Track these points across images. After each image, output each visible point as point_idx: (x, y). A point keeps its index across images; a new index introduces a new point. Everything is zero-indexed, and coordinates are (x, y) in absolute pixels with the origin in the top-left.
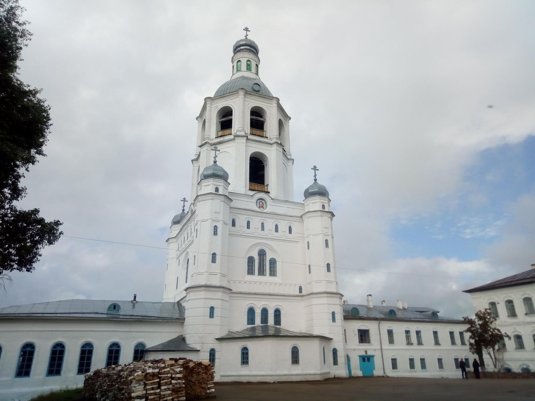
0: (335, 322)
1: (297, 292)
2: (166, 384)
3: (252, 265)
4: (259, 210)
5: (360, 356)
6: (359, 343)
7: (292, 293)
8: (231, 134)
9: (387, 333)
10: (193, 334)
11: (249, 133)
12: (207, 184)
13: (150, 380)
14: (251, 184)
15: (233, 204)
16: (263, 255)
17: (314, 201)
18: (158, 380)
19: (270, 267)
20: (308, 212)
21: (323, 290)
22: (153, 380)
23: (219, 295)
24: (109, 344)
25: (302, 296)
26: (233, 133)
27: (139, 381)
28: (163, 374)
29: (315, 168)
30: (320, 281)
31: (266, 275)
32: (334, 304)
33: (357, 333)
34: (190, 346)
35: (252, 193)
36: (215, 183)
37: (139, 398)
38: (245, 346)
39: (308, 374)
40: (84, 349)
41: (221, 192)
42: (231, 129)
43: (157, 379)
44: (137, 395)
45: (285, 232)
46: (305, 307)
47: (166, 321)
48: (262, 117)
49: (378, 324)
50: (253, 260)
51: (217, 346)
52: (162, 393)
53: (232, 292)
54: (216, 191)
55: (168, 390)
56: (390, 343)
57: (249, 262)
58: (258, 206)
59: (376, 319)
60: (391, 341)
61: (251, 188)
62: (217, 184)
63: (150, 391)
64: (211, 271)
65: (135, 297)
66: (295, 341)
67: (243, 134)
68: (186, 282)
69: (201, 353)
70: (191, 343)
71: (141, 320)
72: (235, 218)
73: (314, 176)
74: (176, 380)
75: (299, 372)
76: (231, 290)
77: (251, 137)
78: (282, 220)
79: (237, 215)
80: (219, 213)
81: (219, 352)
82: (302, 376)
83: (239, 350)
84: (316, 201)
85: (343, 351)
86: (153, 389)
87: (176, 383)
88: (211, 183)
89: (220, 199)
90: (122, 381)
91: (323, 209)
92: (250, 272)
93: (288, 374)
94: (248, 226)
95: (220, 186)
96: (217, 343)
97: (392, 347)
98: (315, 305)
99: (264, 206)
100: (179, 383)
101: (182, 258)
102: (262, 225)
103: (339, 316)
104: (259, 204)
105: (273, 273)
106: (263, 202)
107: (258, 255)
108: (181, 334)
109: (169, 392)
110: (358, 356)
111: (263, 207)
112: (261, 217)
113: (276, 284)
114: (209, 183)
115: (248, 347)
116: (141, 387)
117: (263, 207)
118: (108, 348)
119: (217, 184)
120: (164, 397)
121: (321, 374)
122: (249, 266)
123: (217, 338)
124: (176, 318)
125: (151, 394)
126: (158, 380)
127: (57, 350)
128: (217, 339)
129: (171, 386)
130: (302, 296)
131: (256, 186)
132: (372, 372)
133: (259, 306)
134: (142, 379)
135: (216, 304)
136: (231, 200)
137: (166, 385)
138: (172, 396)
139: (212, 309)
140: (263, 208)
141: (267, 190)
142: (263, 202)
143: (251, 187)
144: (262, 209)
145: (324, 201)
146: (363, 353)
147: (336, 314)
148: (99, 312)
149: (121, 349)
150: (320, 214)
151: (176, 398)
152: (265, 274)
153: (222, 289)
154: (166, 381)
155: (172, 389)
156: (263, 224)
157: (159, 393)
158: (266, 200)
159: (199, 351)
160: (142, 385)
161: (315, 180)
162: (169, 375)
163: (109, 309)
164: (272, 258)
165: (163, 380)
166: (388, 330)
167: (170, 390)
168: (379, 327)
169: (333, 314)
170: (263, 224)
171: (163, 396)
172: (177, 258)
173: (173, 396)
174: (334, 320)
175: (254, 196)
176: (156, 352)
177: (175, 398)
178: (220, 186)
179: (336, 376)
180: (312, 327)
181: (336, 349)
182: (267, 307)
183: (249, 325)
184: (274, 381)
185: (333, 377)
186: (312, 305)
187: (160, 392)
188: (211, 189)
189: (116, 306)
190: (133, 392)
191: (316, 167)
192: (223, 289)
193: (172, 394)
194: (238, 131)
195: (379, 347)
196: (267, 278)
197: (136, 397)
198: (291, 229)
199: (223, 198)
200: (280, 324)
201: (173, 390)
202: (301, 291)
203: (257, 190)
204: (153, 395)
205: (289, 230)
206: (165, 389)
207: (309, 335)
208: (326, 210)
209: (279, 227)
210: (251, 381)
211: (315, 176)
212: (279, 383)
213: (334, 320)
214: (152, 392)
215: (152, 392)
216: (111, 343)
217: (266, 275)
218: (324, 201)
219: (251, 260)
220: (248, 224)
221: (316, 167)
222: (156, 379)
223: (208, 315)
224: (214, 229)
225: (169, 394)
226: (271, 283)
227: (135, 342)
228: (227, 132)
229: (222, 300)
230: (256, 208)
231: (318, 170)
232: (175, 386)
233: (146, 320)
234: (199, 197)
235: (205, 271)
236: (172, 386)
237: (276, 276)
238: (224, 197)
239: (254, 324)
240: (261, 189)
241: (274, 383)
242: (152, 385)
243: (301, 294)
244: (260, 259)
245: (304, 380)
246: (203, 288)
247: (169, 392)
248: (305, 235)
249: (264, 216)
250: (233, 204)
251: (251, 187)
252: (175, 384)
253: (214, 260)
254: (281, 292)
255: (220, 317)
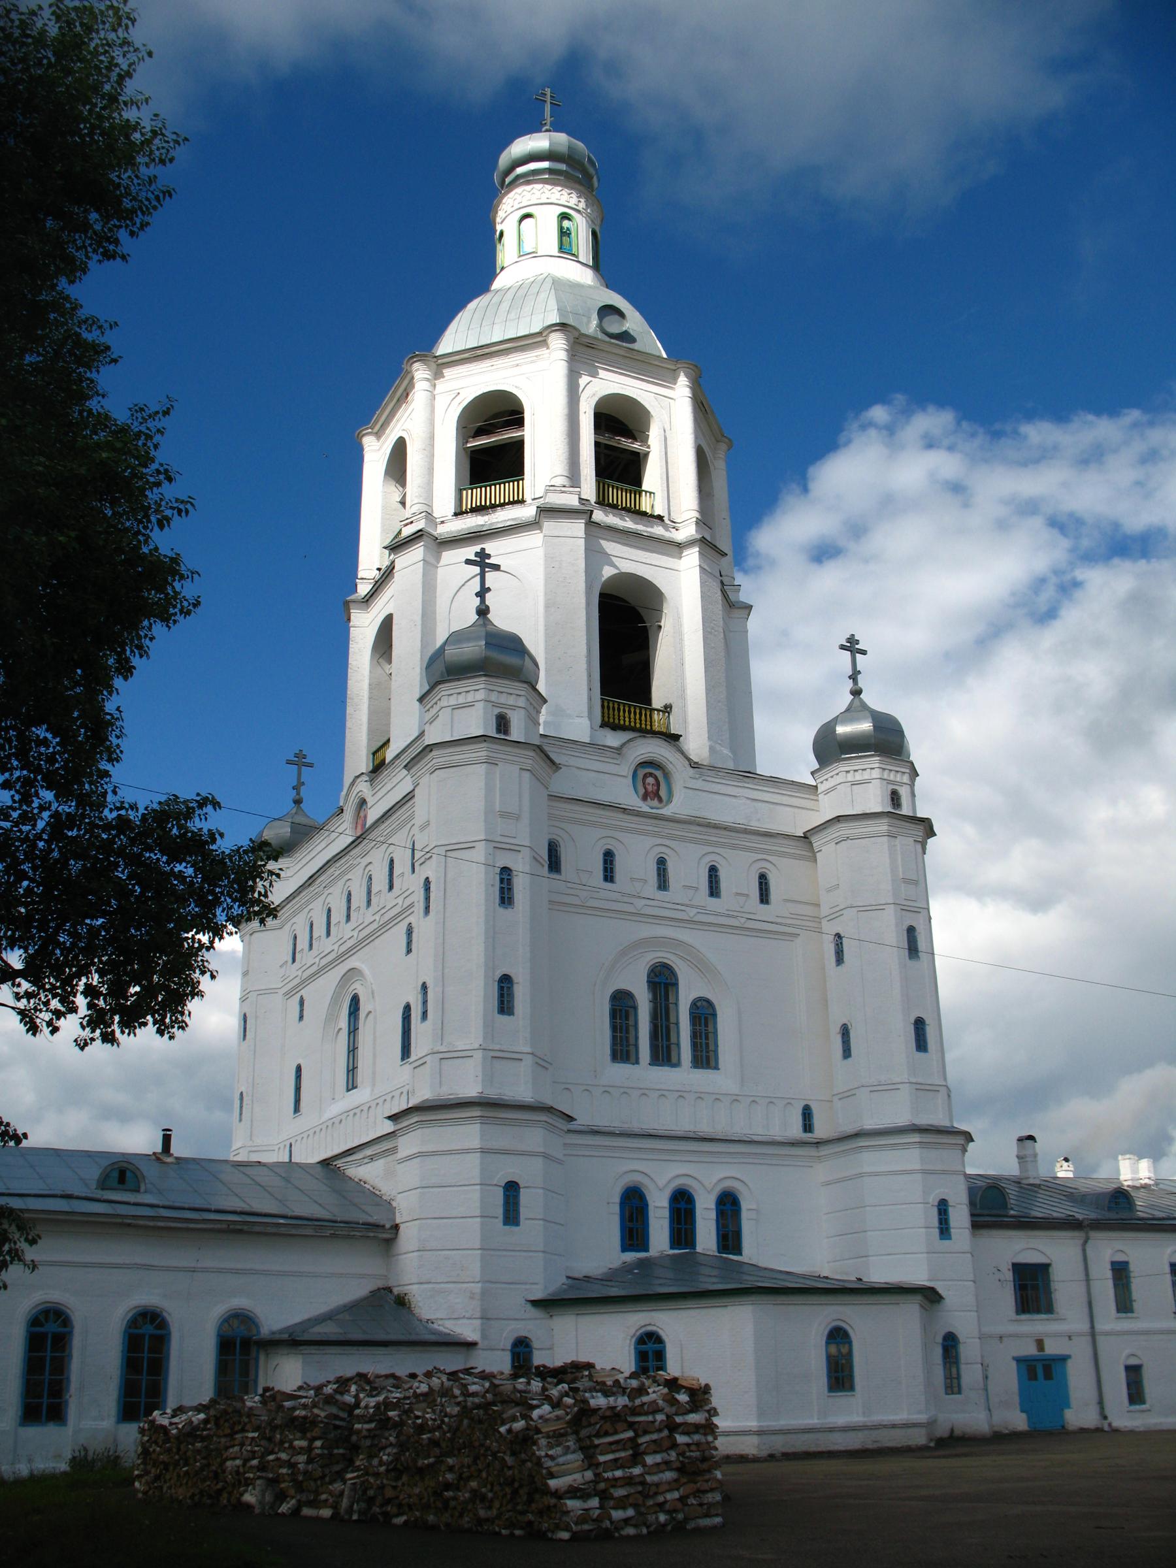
0: (950, 1239)
1: (795, 1130)
2: (657, 1447)
3: (627, 1026)
4: (644, 807)
5: (1019, 1360)
6: (1018, 1313)
7: (777, 1131)
8: (521, 502)
9: (1109, 1274)
10: (442, 1285)
11: (593, 499)
12: (461, 699)
13: (606, 1434)
14: (606, 704)
15: (562, 784)
16: (667, 985)
17: (858, 777)
18: (630, 1434)
19: (695, 1035)
20: (838, 819)
21: (903, 1120)
22: (616, 1432)
23: (534, 1137)
24: (126, 1314)
25: (818, 1144)
26: (528, 497)
27: (557, 1437)
28: (640, 1414)
29: (852, 646)
30: (892, 1087)
31: (677, 1064)
32: (944, 1172)
33: (1009, 1275)
34: (435, 1326)
35: (613, 739)
36: (494, 697)
37: (578, 1494)
38: (650, 1328)
39: (885, 1426)
40: (136, 1331)
41: (516, 734)
42: (523, 479)
43: (625, 1431)
44: (571, 1486)
45: (747, 895)
46: (828, 1184)
47: (328, 1233)
48: (631, 435)
49: (1081, 1242)
50: (631, 1003)
51: (534, 1326)
52: (648, 1478)
53: (573, 1126)
54: (499, 731)
55: (663, 1467)
56: (1118, 1311)
57: (614, 1014)
58: (642, 791)
59: (1070, 1224)
60: (1124, 1304)
61: (606, 719)
62: (503, 699)
63: (612, 1470)
64: (497, 1047)
65: (167, 1140)
66: (840, 1308)
67: (572, 501)
68: (351, 1086)
69: (481, 1352)
70: (439, 1315)
71: (239, 1227)
72: (558, 839)
73: (850, 677)
74: (687, 1433)
75: (857, 1419)
76: (570, 1118)
77: (599, 516)
78: (734, 847)
79: (562, 825)
80: (518, 818)
81: (544, 1352)
82: (866, 1432)
83: (628, 1341)
84: (866, 775)
85: (977, 1340)
86: (616, 1464)
87: (688, 1445)
88: (481, 695)
89: (522, 760)
90: (425, 1442)
91: (894, 808)
92: (623, 1051)
93: (819, 1426)
94: (605, 870)
95: (513, 708)
96: (536, 1319)
97: (1126, 1324)
98: (876, 1174)
99: (663, 793)
100: (698, 1444)
101: (321, 993)
102: (659, 869)
103: (960, 1217)
104: (644, 783)
105: (705, 1057)
106: (658, 773)
107: (649, 986)
108: (380, 1284)
109: (669, 1475)
110: (1015, 1359)
111: (656, 795)
112: (655, 835)
113: (664, 1093)
114: (470, 697)
115: (661, 1333)
116: (570, 1457)
117: (656, 795)
118: (123, 1329)
119: (503, 699)
120: (656, 1494)
121: (760, 1433)
122: (614, 1028)
123: (533, 1299)
124: (362, 1224)
125: (615, 1482)
126: (630, 1434)
127: (143, 1335)
128: (536, 1303)
129: (673, 1455)
130: (818, 1144)
131: (627, 712)
132: (1062, 1416)
133: (662, 1182)
134: (562, 1431)
135: (527, 1172)
136: (554, 765)
137: (658, 1450)
138: (678, 1489)
139: (512, 1189)
140: (660, 800)
141: (668, 726)
142: (658, 773)
143: (606, 715)
144: (655, 803)
145: (898, 778)
146: (1031, 1350)
147: (950, 1210)
148: (76, 1194)
149: (169, 1334)
150: (484, 753)
151: (691, 1497)
152: (674, 1060)
153: (543, 1117)
154: (655, 1436)
155: (678, 1465)
156: (661, 863)
157: (641, 1479)
158: (670, 767)
159: (472, 1345)
160: (574, 1452)
161: (857, 693)
162: (660, 1417)
163: (103, 1184)
164: (700, 999)
165: (646, 1432)
166: (1113, 1263)
167: (671, 1470)
168: (1084, 1251)
169: (943, 1208)
170: (661, 863)
171: (653, 1489)
172: (286, 994)
173: (681, 1489)
174: (944, 1230)
175: (625, 750)
176: (321, 1347)
177: (687, 1497)
178: (513, 708)
179: (957, 1432)
180: (864, 1259)
181: (952, 1333)
182: (689, 1186)
183: (627, 1253)
184: (769, 1452)
185: (946, 1434)
186: (861, 1175)
187: (642, 1475)
188: (476, 722)
189: (128, 1174)
190: (552, 1476)
191: (857, 642)
192: (550, 1115)
193: (676, 1481)
194: (551, 488)
195: (1085, 1327)
196: (684, 1075)
197: (567, 1492)
198: (766, 883)
199: (529, 759)
200: (738, 1250)
201: (681, 1470)
202: (810, 1125)
203: (633, 729)
204: (622, 1486)
205: (761, 889)
206: (658, 1464)
207: (889, 1286)
208: (905, 810)
209: (723, 875)
210: (1085, 1427)
211: (854, 677)
212: (787, 1456)
213: (944, 1230)
214: (618, 1473)
215: (618, 1473)
216: (134, 1311)
217: (677, 1064)
218: (898, 778)
219: (622, 1005)
220: (605, 862)
221: (857, 642)
222: (622, 1432)
223: (500, 1211)
224: (502, 881)
225: (669, 1483)
226: (702, 1095)
227: (219, 1310)
228: (499, 491)
229: (546, 1156)
230: (632, 800)
231: (864, 652)
232: (688, 1454)
233: (257, 1229)
234: (434, 753)
235: (477, 1046)
236: (678, 1455)
237: (716, 1068)
238: (532, 754)
239: (646, 1250)
240: (643, 722)
241: (771, 1457)
242: (613, 1452)
243: (810, 1135)
244: (654, 1001)
245: (870, 1446)
246: (476, 1112)
247: (669, 1475)
248: (825, 910)
249: (667, 831)
250: (562, 784)
251: (606, 715)
252: (686, 1448)
253: (505, 1004)
254: (740, 1129)
255: (541, 1222)
